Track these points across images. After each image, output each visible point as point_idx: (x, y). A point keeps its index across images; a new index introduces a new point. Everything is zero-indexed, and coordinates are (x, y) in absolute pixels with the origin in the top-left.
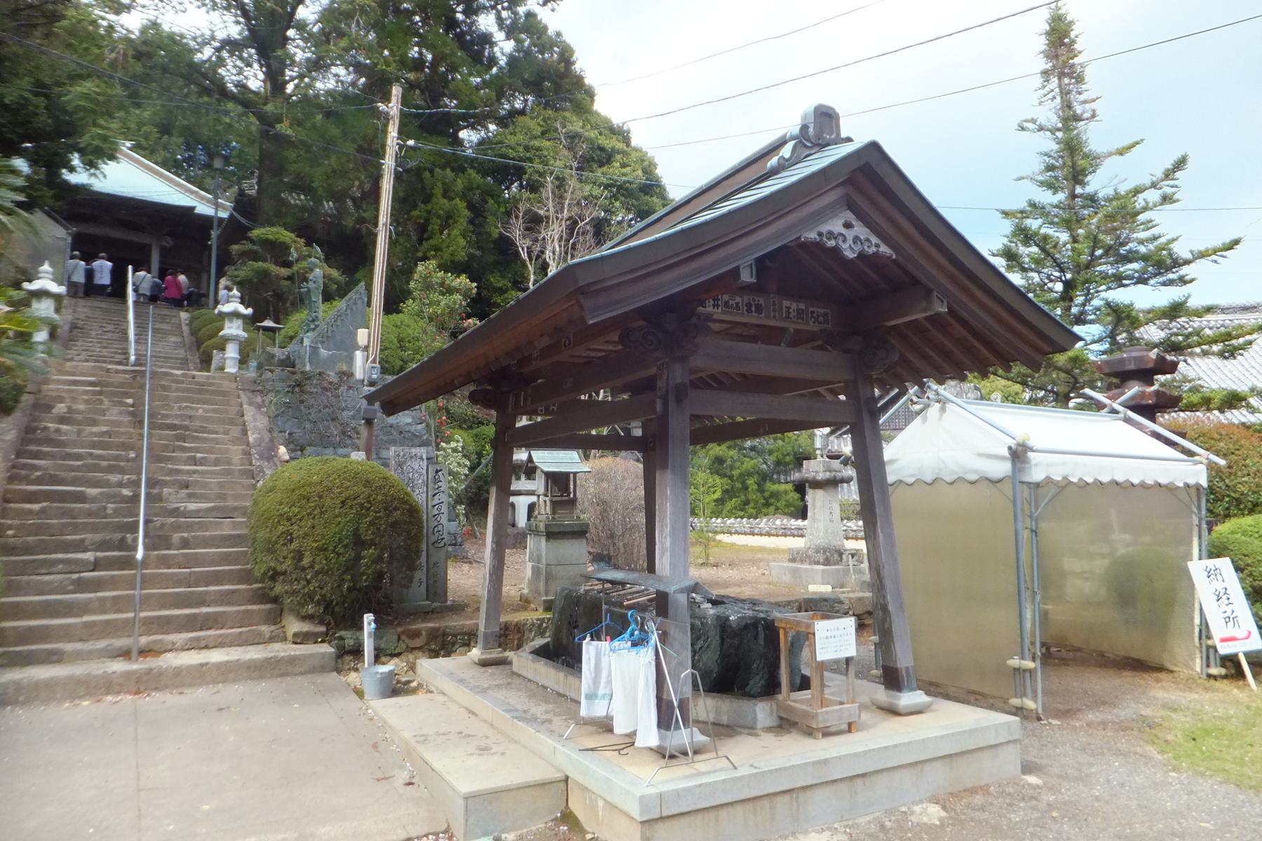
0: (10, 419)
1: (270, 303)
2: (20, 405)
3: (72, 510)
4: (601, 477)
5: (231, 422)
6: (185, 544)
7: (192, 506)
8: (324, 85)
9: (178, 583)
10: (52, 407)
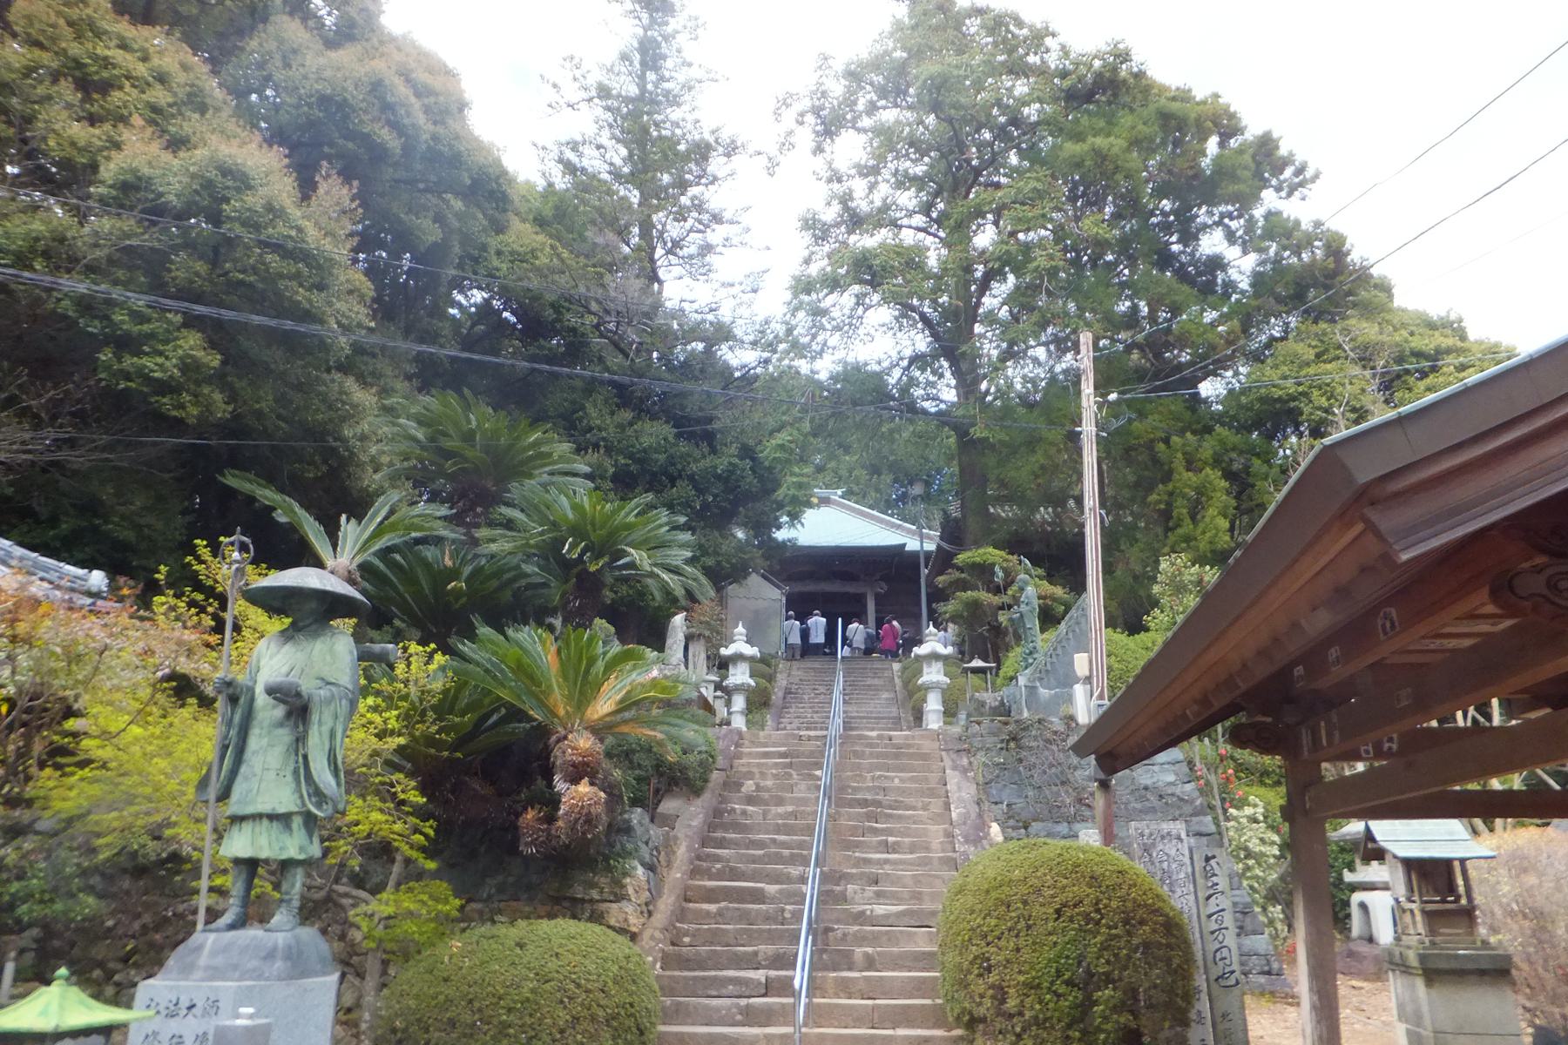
0: (699, 802)
1: (986, 641)
2: (710, 785)
3: (748, 912)
4: (1520, 865)
5: (932, 793)
6: (870, 963)
7: (880, 910)
8: (1016, 374)
9: (858, 1022)
10: (741, 785)
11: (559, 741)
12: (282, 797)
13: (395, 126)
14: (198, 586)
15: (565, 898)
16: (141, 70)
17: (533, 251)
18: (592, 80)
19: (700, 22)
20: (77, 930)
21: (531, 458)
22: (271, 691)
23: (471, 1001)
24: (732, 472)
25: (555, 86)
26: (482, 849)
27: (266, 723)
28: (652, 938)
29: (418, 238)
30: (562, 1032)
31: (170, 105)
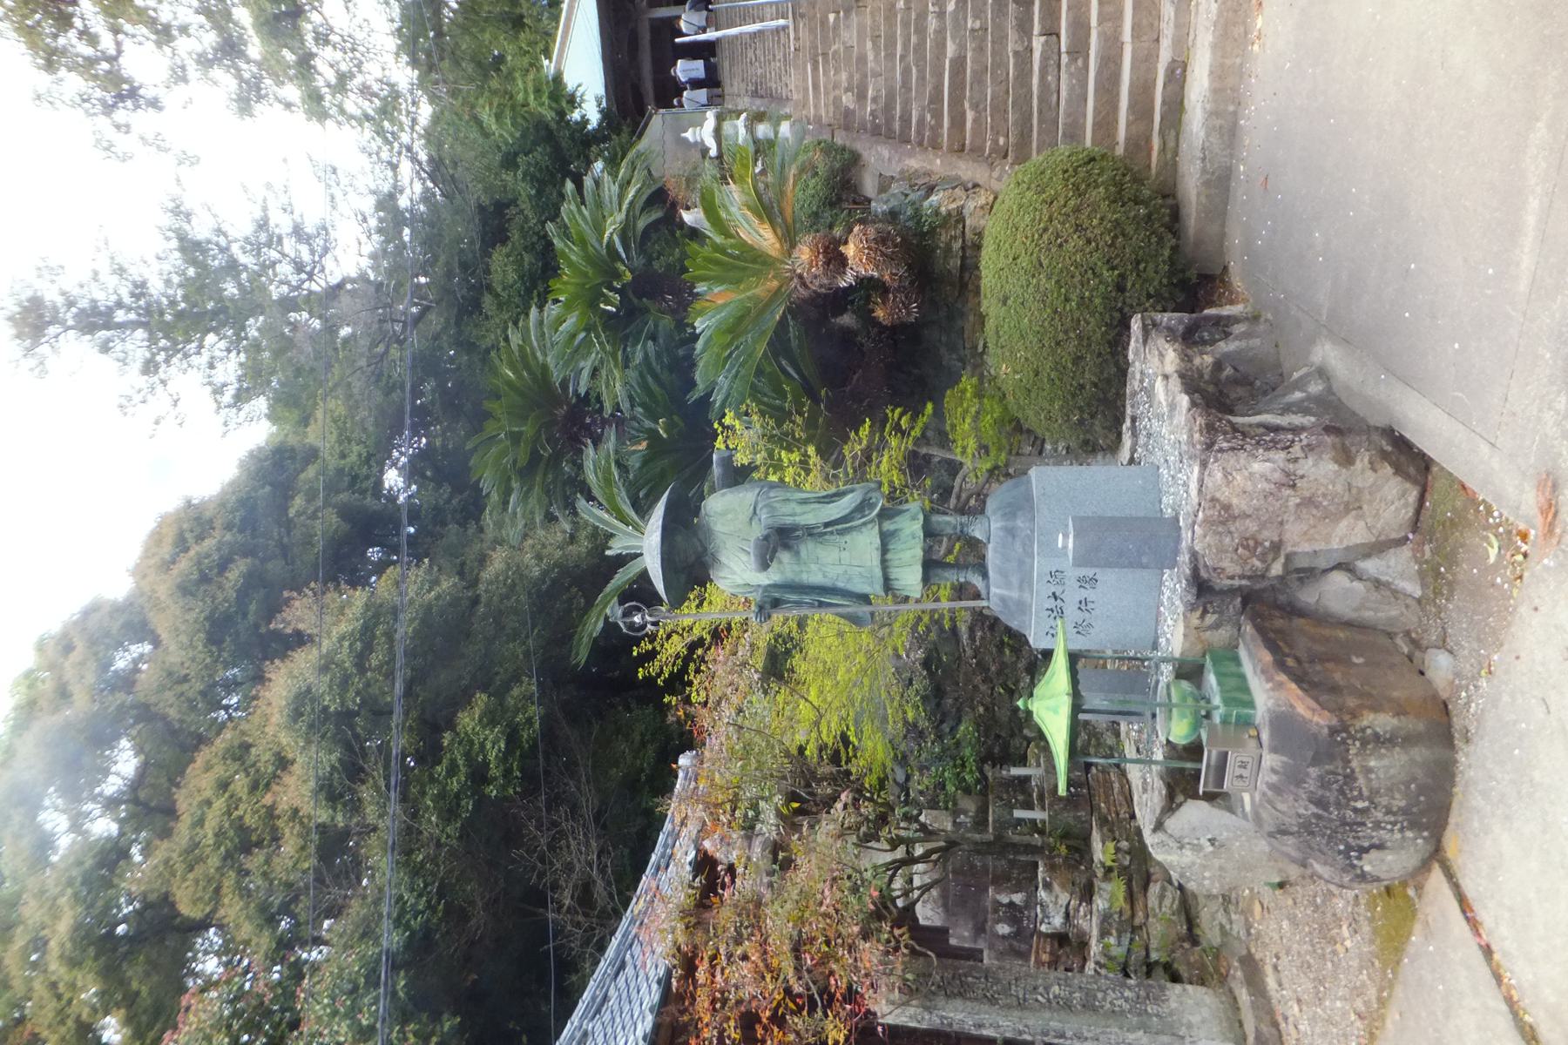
2: (848, 144)
11: (804, 284)
12: (866, 542)
13: (223, 566)
14: (684, 670)
15: (961, 277)
16: (220, 804)
17: (335, 421)
18: (143, 382)
19: (41, 264)
20: (987, 736)
21: (530, 372)
22: (764, 565)
23: (1058, 344)
24: (533, 177)
25: (157, 423)
26: (916, 371)
27: (796, 568)
28: (999, 179)
29: (336, 531)
30: (1089, 242)
31: (248, 775)
